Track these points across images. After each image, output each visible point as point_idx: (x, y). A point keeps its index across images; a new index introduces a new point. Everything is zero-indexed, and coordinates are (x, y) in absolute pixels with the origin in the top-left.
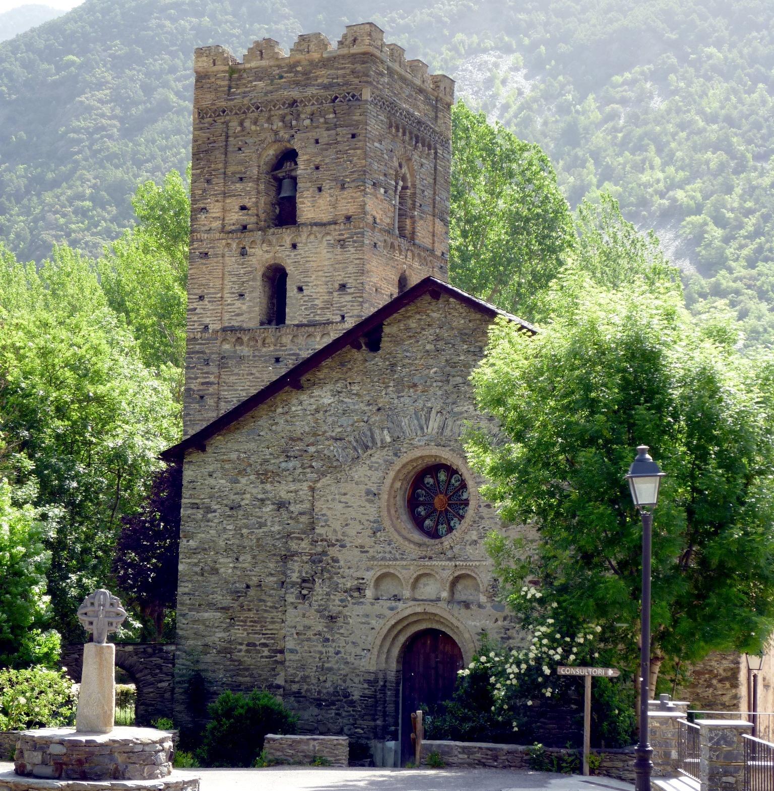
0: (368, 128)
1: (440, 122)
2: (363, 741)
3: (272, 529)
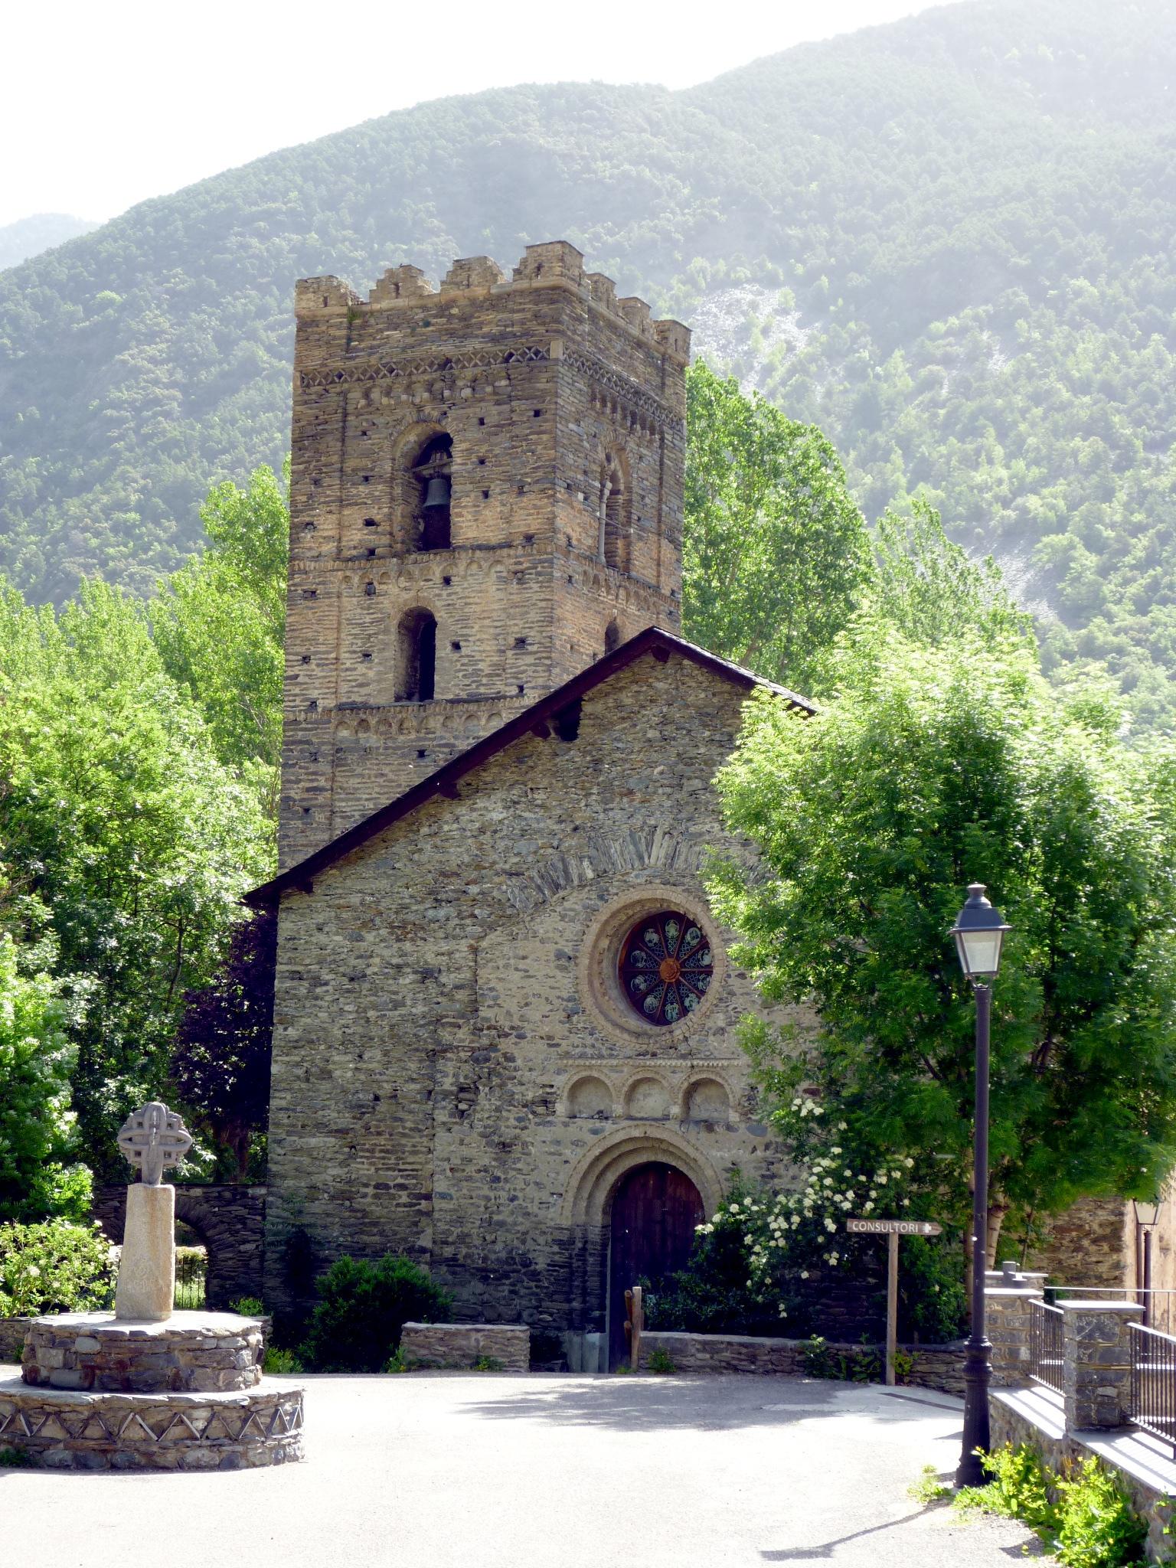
0: (559, 401)
1: (668, 391)
2: (552, 1334)
3: (414, 1010)
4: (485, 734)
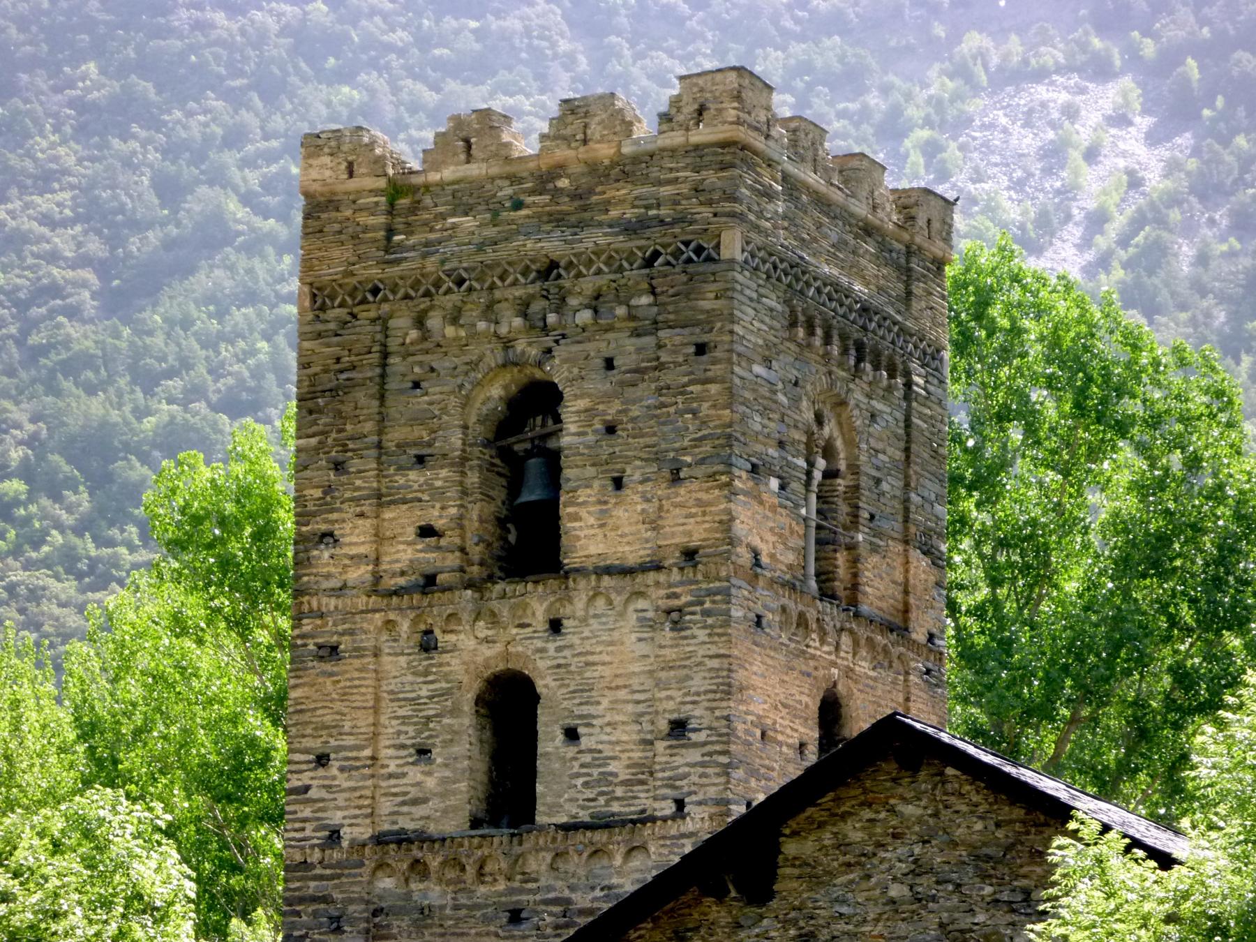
0: (737, 328)
1: (916, 305)
4: (628, 886)
